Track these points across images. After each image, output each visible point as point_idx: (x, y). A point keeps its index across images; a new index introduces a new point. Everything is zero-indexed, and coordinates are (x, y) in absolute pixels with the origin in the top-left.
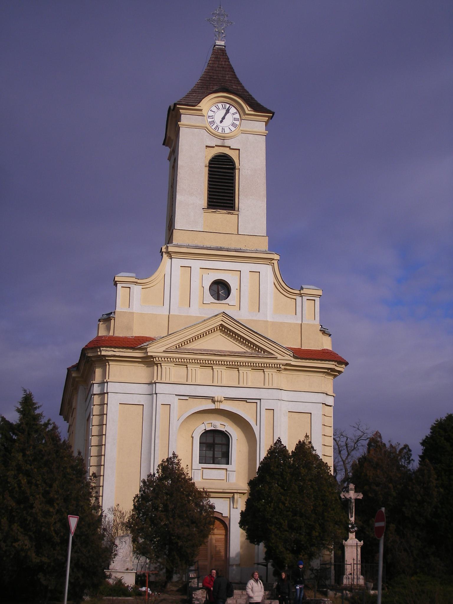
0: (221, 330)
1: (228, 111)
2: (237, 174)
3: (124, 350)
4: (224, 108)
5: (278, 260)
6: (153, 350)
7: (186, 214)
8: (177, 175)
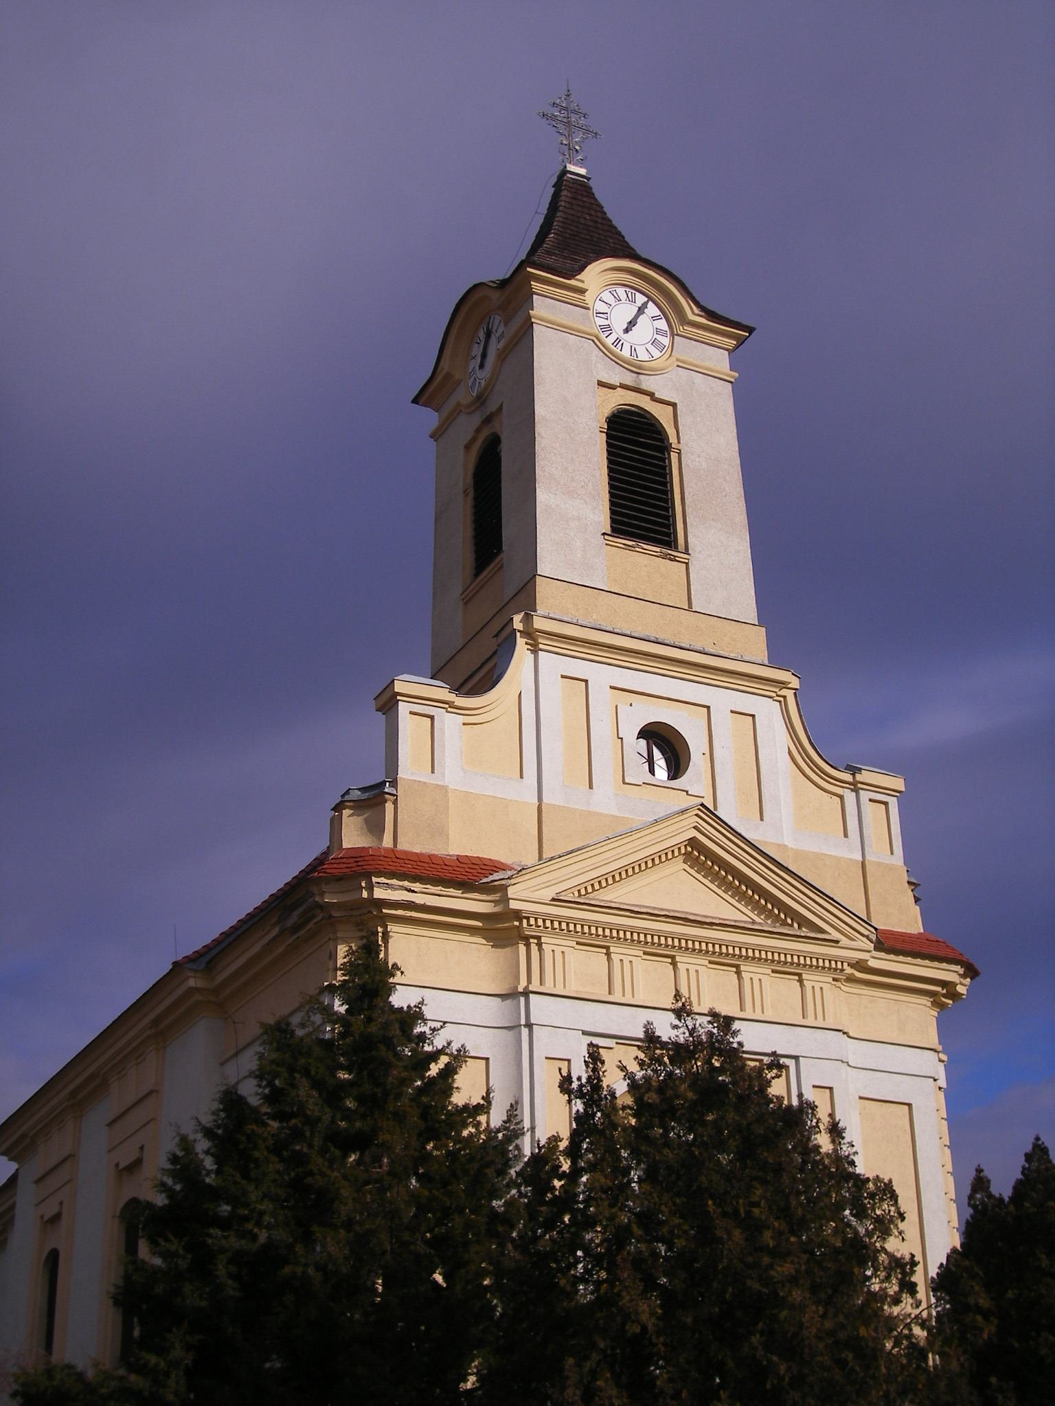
0: (688, 857)
1: (641, 310)
2: (675, 463)
3: (437, 888)
4: (631, 300)
5: (796, 689)
6: (524, 895)
7: (562, 541)
8: (535, 438)
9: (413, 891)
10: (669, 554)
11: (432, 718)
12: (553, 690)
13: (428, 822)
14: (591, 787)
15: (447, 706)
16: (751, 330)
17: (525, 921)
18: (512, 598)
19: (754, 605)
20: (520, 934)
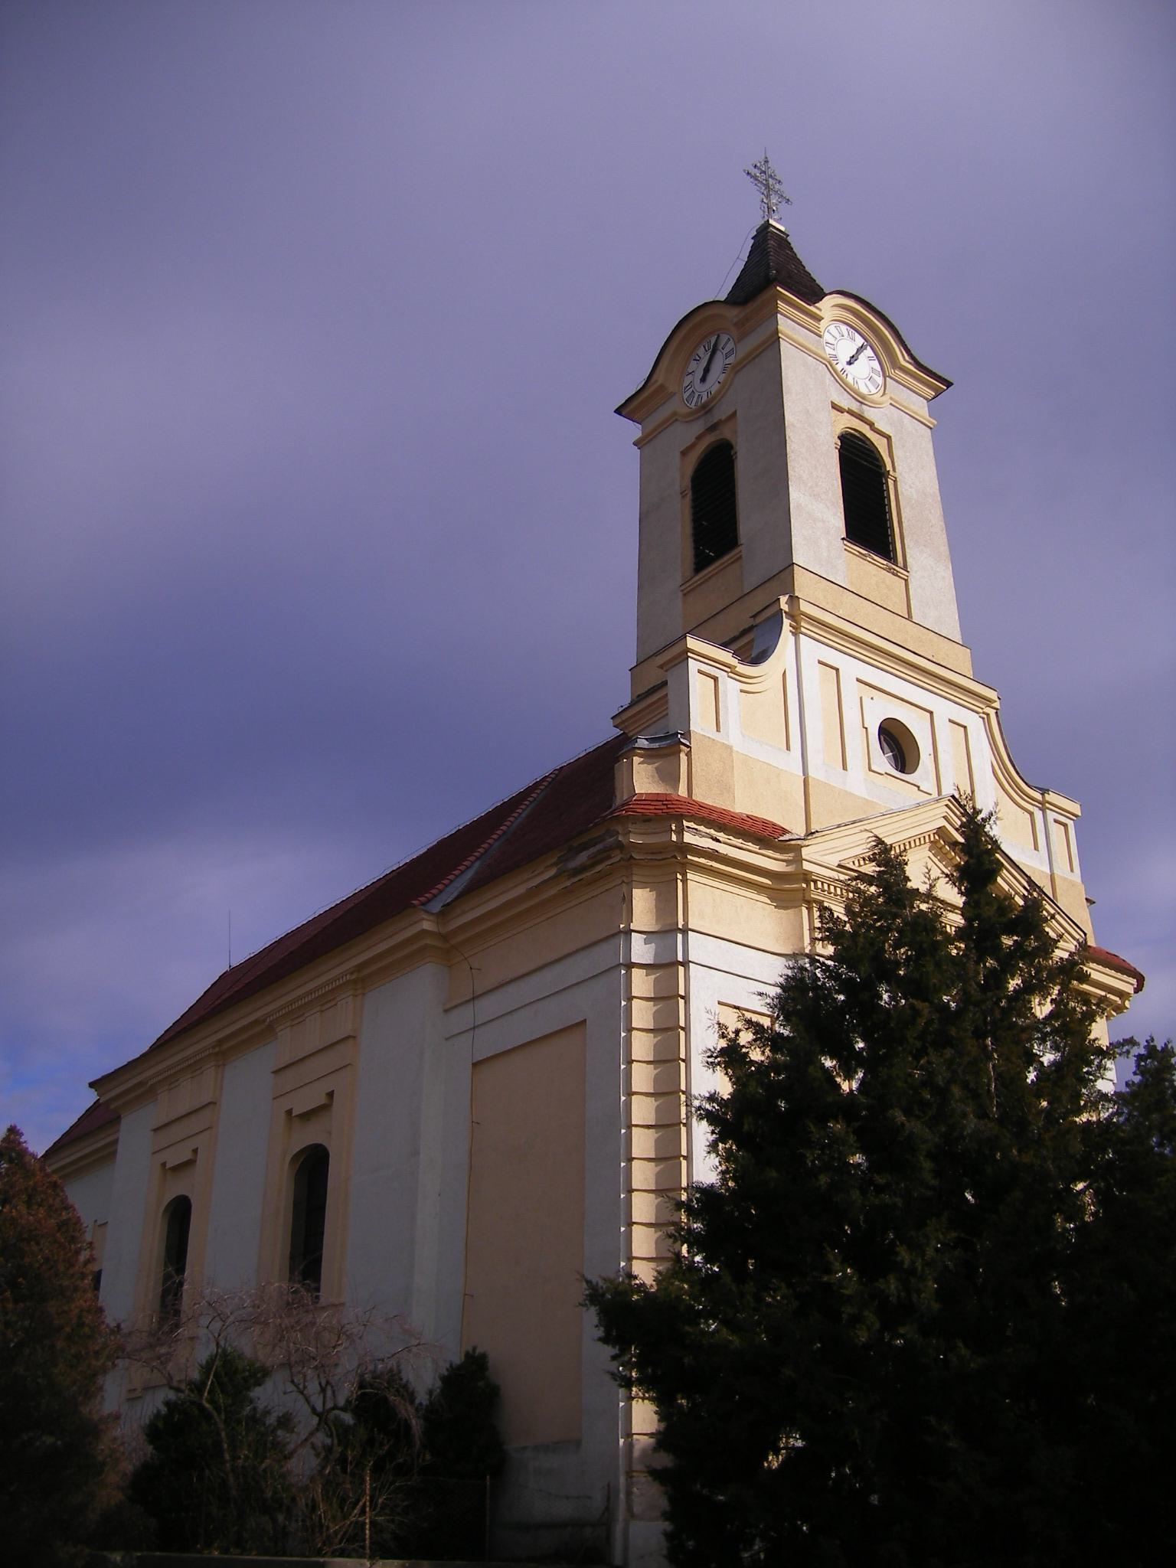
9: (718, 841)
10: (894, 570)
11: (715, 679)
12: (813, 675)
13: (718, 778)
14: (845, 768)
15: (729, 670)
16: (949, 384)
17: (812, 884)
18: (760, 585)
19: (959, 629)
20: (804, 897)
